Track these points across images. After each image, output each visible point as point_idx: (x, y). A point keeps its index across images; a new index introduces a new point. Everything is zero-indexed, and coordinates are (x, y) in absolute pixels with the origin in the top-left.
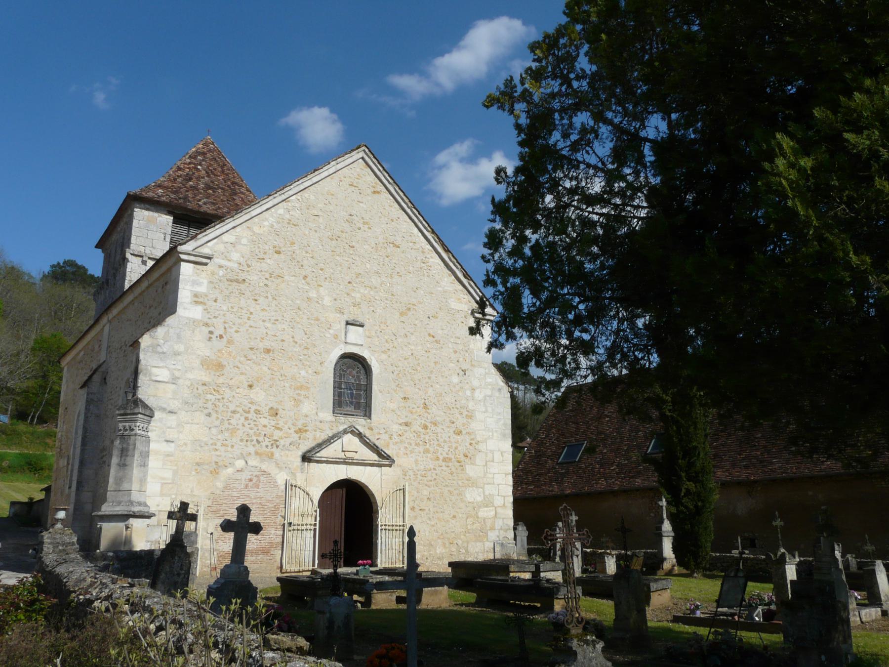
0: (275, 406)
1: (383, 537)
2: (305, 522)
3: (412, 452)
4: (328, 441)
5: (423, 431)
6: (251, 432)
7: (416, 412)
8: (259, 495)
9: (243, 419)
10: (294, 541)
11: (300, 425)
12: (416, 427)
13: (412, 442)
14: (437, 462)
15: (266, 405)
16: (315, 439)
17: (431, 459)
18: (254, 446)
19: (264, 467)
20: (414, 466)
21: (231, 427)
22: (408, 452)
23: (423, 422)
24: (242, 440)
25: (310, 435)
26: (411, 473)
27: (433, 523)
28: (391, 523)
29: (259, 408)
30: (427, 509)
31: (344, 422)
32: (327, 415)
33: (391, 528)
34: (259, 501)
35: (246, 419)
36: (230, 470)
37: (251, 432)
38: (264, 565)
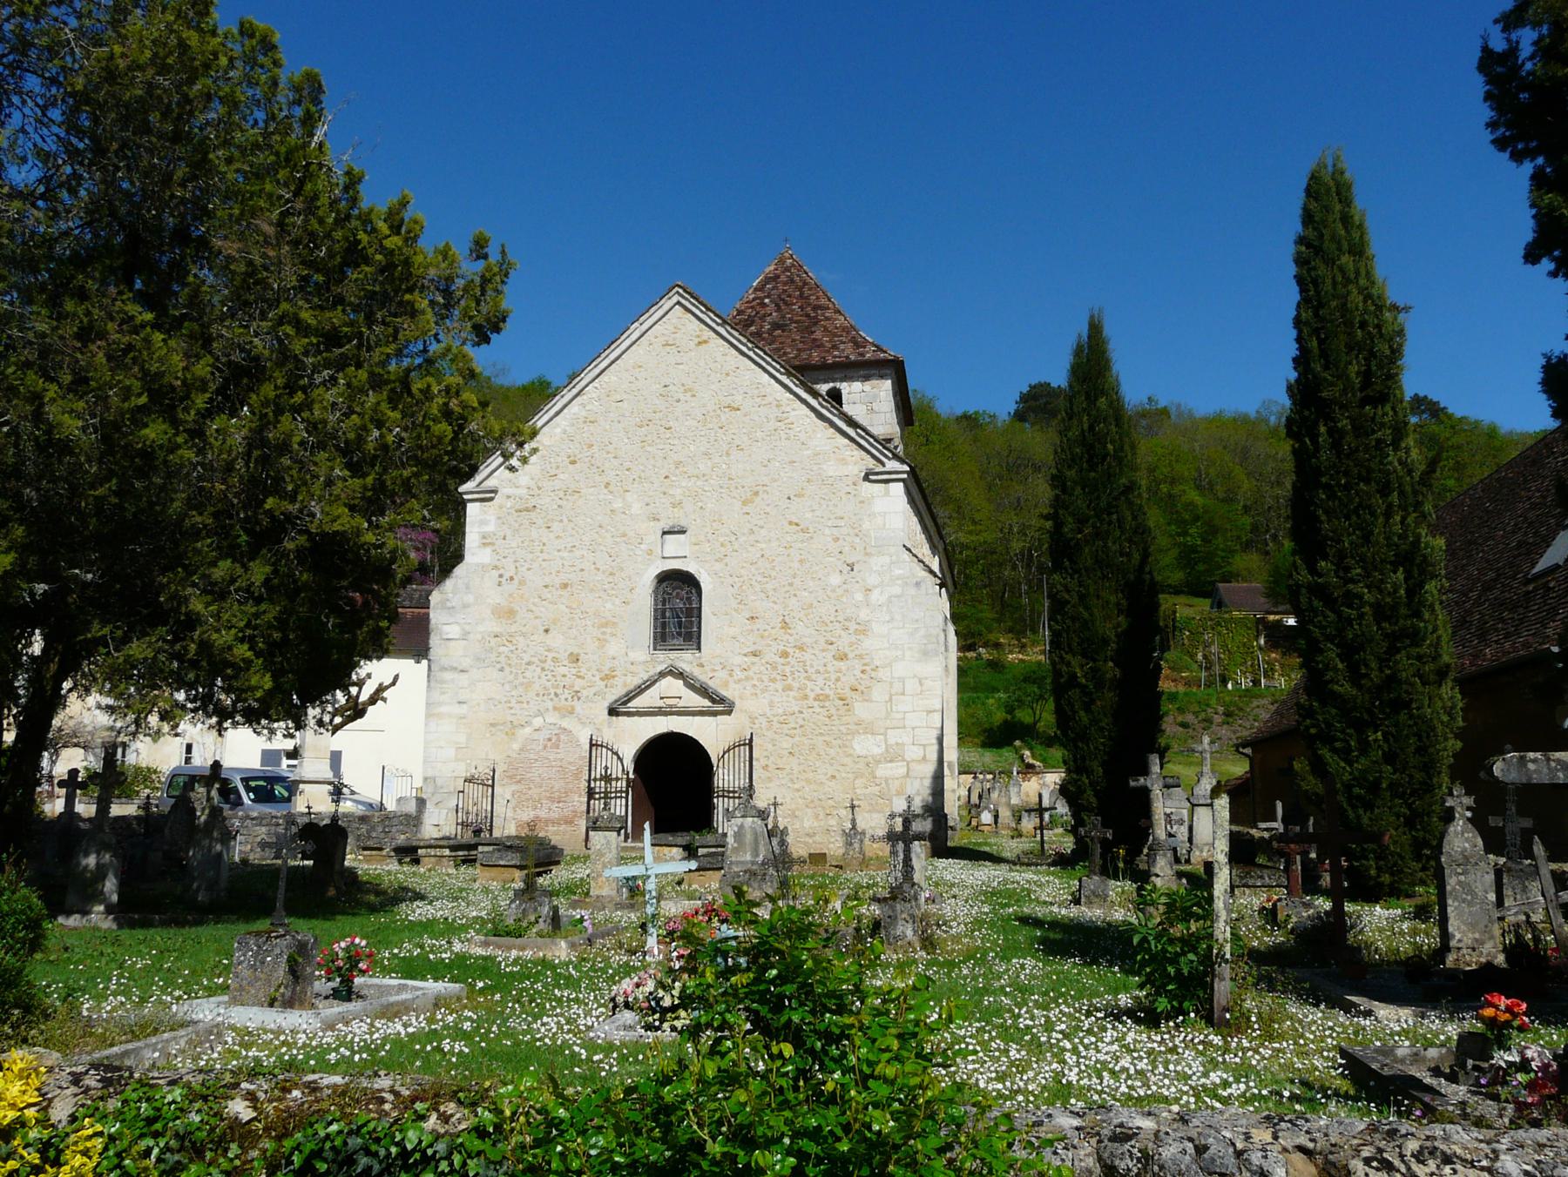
3: (764, 691)
4: (640, 690)
5: (782, 660)
12: (769, 656)
16: (625, 685)
19: (565, 723)
25: (618, 681)
31: (665, 659)
36: (528, 730)
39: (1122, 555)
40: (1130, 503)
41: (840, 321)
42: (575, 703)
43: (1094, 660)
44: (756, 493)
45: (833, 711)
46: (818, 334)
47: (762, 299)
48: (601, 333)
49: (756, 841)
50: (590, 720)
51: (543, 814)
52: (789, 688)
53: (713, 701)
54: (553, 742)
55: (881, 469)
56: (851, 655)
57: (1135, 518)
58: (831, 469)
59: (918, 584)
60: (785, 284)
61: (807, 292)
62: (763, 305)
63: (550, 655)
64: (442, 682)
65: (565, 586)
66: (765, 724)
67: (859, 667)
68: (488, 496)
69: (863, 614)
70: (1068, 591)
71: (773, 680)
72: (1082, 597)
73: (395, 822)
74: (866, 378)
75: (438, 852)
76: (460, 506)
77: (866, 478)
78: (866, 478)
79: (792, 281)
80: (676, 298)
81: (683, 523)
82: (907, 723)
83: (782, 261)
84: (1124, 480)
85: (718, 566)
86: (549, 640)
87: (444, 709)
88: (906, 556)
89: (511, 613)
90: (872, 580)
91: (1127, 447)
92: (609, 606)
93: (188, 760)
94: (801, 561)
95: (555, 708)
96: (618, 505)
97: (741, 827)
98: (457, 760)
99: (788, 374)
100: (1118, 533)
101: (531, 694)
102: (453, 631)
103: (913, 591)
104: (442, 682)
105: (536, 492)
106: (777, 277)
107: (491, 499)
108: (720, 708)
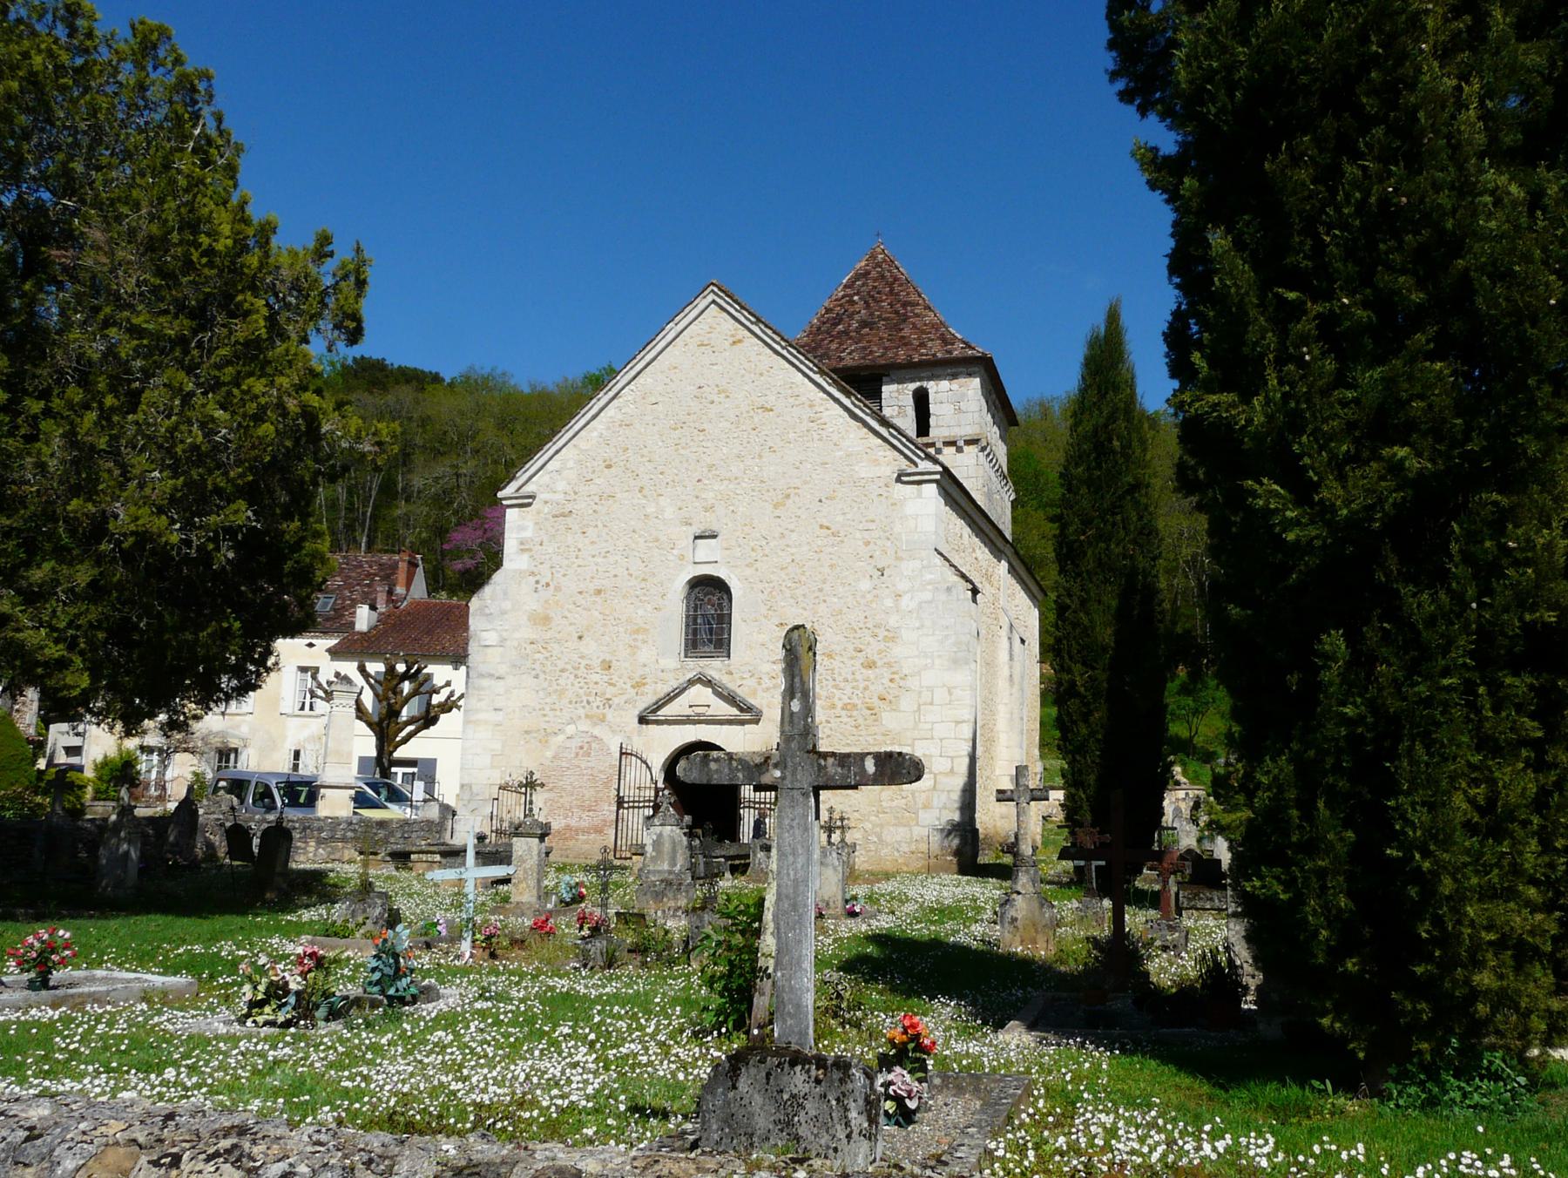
4: (670, 698)
19: (596, 731)
25: (648, 689)
31: (695, 666)
36: (561, 738)
39: (1125, 558)
40: (1136, 503)
41: (930, 317)
43: (1093, 668)
44: (788, 496)
45: (861, 721)
46: (906, 332)
47: (851, 296)
48: (642, 330)
49: (674, 851)
50: (621, 729)
51: (573, 823)
53: (742, 710)
54: (584, 751)
55: (914, 470)
56: (879, 664)
57: (1141, 518)
58: (864, 471)
59: (949, 589)
60: (875, 280)
61: (897, 288)
62: (852, 303)
63: (584, 662)
64: (479, 689)
65: (599, 592)
67: (888, 676)
68: (526, 502)
69: (893, 621)
70: (1070, 596)
72: (1083, 602)
73: (416, 827)
74: (954, 376)
75: (430, 857)
76: (498, 507)
77: (898, 480)
78: (898, 480)
79: (883, 277)
80: (711, 297)
81: (715, 527)
82: (935, 734)
83: (873, 257)
84: (1130, 479)
85: (749, 572)
87: (481, 716)
88: (938, 560)
89: (546, 620)
90: (902, 586)
91: (1135, 444)
92: (640, 612)
93: (296, 767)
94: (831, 566)
95: (587, 716)
96: (651, 510)
97: (660, 835)
98: (492, 767)
99: (822, 372)
100: (1122, 533)
102: (490, 637)
103: (943, 597)
104: (479, 689)
105: (573, 496)
106: (867, 273)
107: (529, 505)
108: (747, 716)
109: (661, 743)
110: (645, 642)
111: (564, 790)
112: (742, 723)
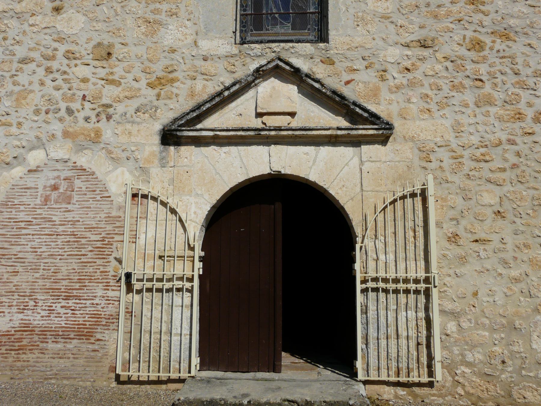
0: (106, 39)
1: (372, 307)
2: (168, 273)
3: (441, 106)
4: (221, 100)
5: (472, 55)
6: (57, 95)
7: (448, 14)
8: (70, 216)
9: (41, 72)
10: (146, 313)
11: (158, 69)
12: (450, 47)
13: (441, 82)
14: (518, 124)
15: (89, 40)
16: (192, 94)
17: (500, 119)
18: (61, 120)
19: (83, 160)
20: (450, 136)
21: (17, 89)
22: (433, 107)
23: (469, 34)
24: (37, 112)
25: (181, 89)
26: (443, 154)
27: (514, 273)
28: (392, 275)
29: (73, 48)
30: (495, 238)
31: (259, 55)
32: (221, 43)
33: (401, 286)
34: (69, 229)
35: (49, 71)
36: (18, 171)
37: (57, 95)
38: (81, 361)
42: (103, 124)
51: (37, 319)
52: (489, 101)
54: (60, 192)
66: (447, 163)
71: (458, 88)
86: (61, 23)
93: (397, 296)
95: (66, 134)
101: (26, 111)
109: (218, 171)
110: (172, 15)
111: (20, 260)
112: (356, 142)
